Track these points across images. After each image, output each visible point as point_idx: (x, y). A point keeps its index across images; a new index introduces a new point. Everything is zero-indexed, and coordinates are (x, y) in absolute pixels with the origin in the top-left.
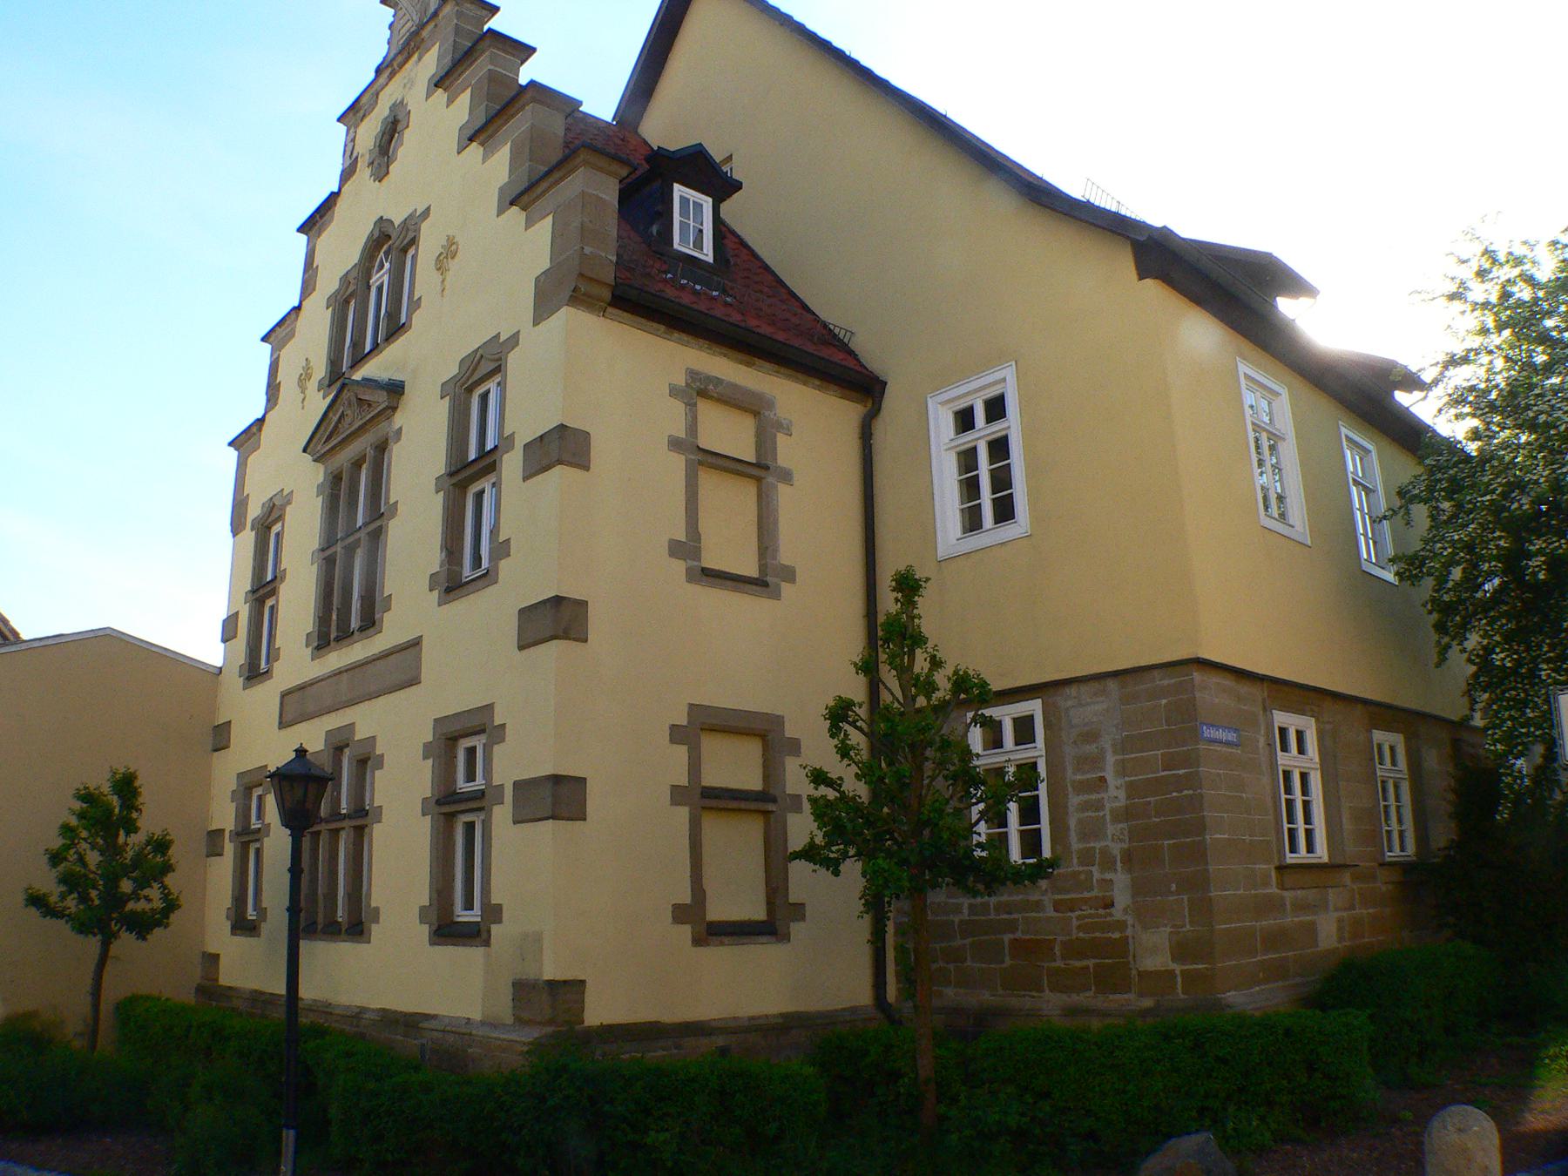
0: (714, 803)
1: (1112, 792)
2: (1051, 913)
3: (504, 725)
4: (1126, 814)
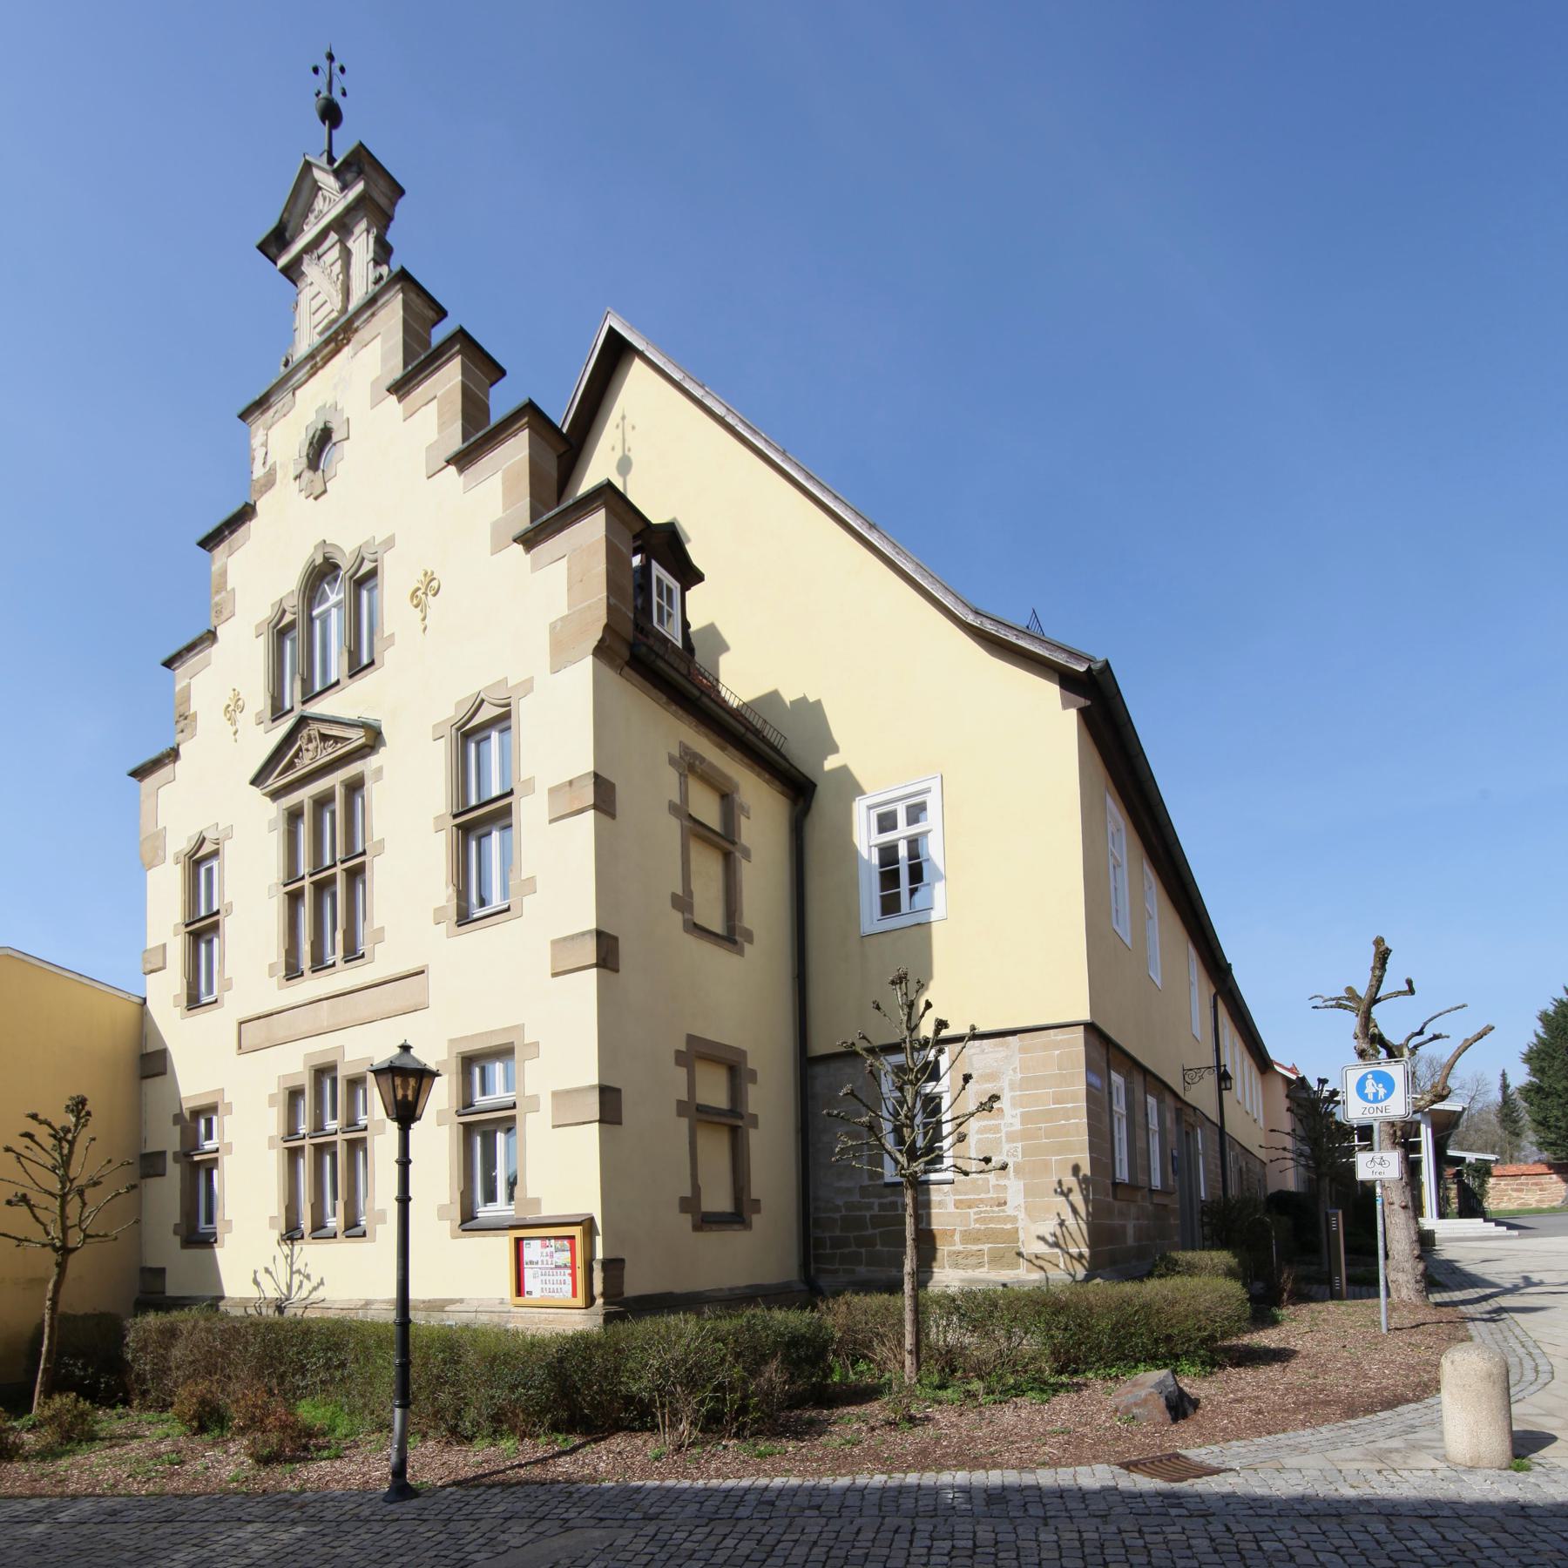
0: (704, 1117)
1: (1008, 1119)
2: (951, 1208)
3: (537, 1044)
4: (1024, 1135)
